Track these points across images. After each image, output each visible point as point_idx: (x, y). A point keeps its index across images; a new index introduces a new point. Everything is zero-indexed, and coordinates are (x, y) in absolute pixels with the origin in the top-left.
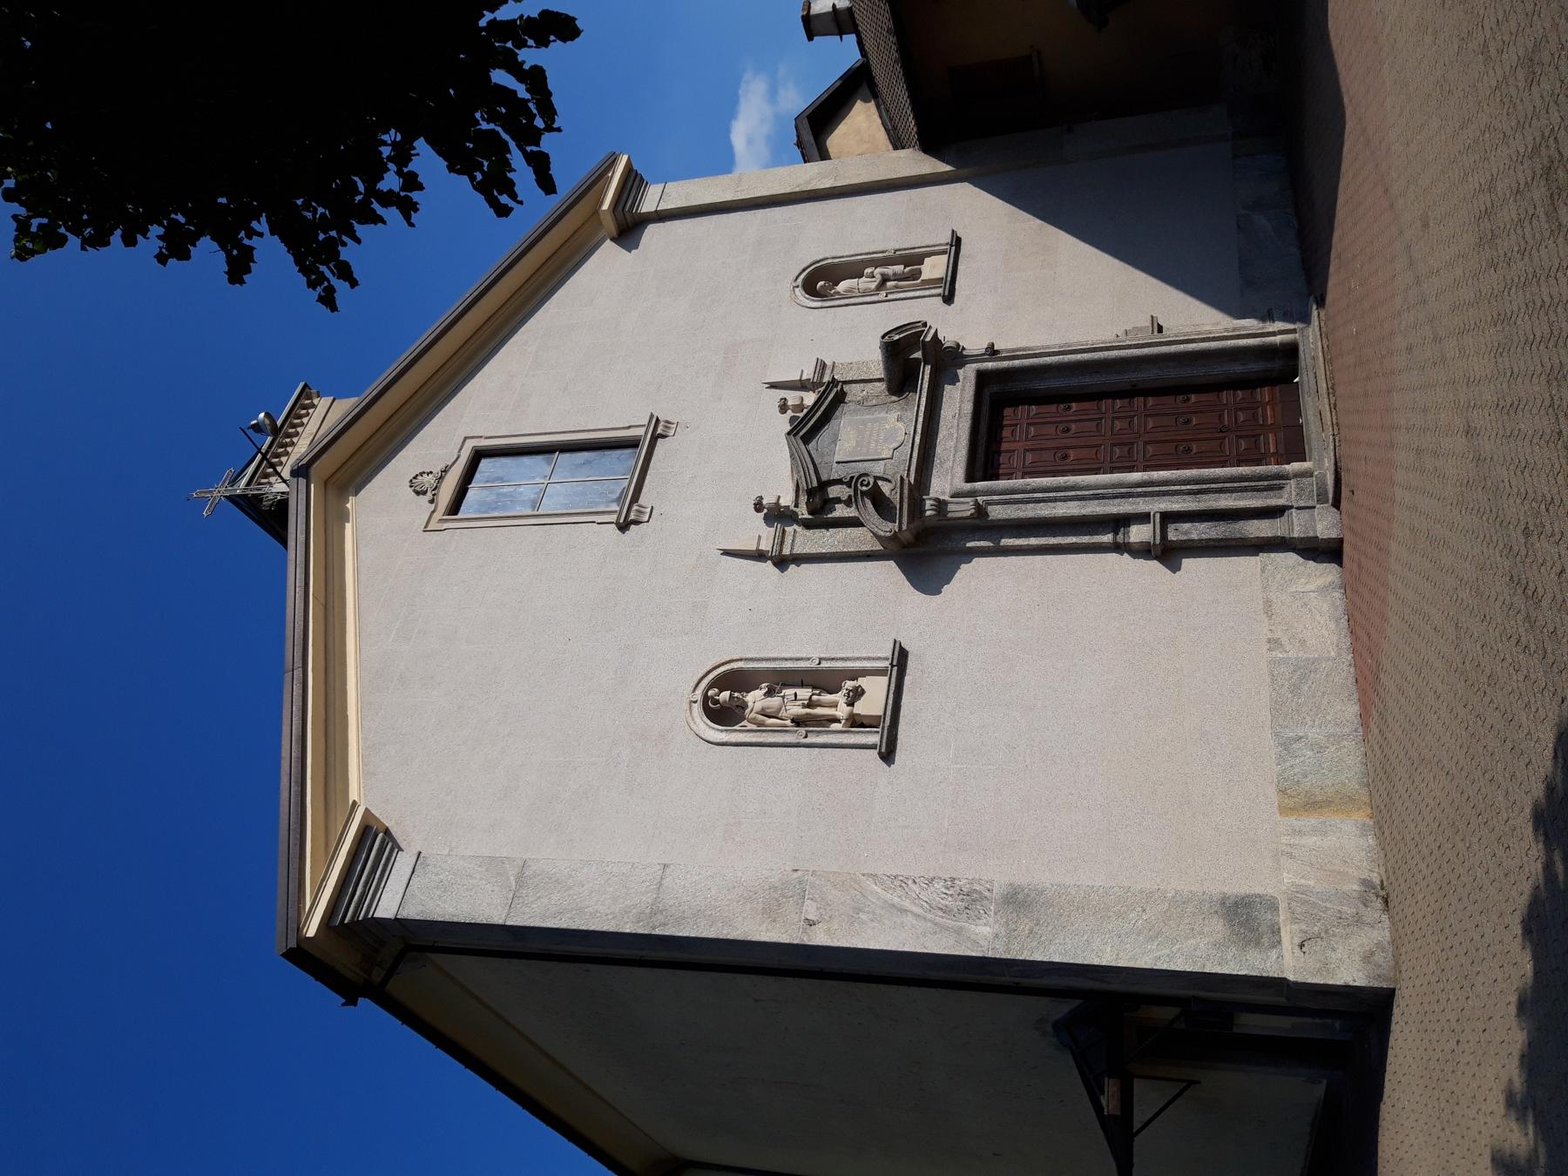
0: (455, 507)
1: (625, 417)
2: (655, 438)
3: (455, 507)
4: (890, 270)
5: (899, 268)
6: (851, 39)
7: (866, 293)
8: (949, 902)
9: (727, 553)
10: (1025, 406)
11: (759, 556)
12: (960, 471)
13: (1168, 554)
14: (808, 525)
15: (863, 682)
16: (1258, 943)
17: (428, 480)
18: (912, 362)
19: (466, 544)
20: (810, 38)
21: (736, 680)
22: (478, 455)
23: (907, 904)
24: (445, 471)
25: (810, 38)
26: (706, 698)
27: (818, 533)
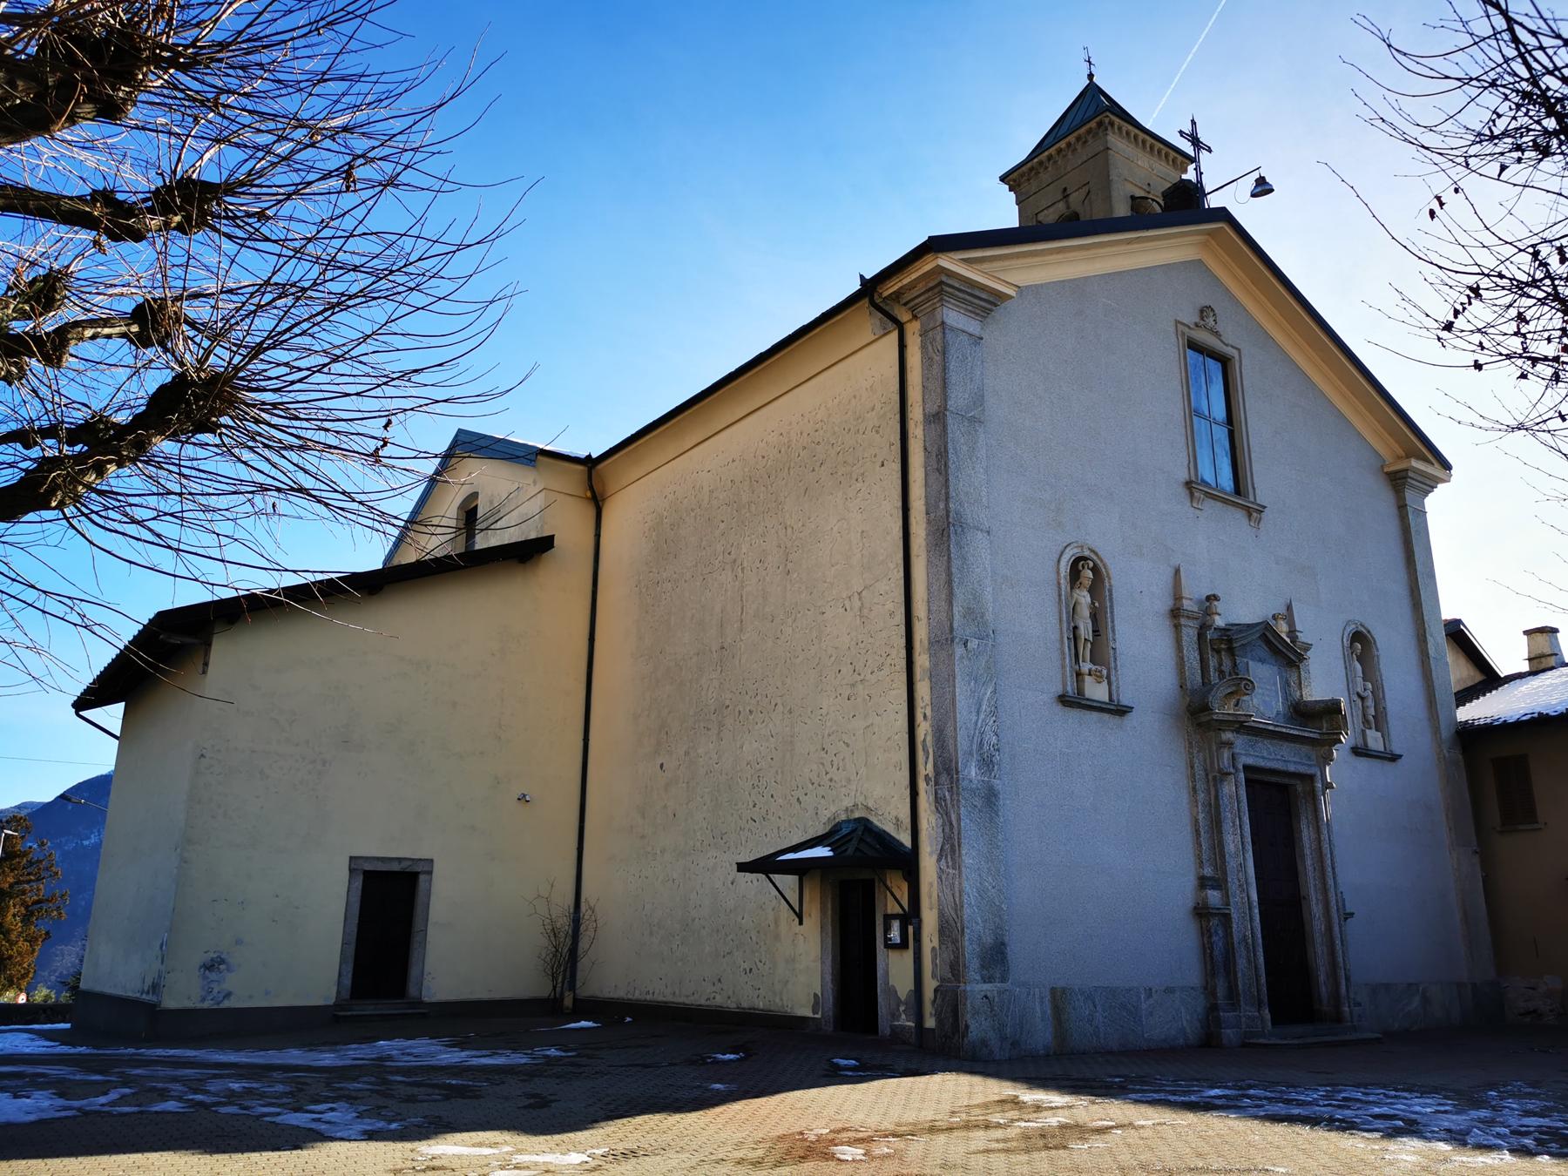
0: (1193, 345)
1: (1265, 482)
2: (1249, 512)
3: (1193, 345)
4: (1370, 703)
5: (1372, 711)
6: (1525, 667)
7: (1355, 683)
8: (986, 747)
9: (1177, 571)
10: (1279, 806)
11: (1178, 597)
12: (1250, 761)
13: (1201, 912)
14: (1201, 636)
15: (1105, 683)
16: (983, 966)
17: (1210, 321)
18: (1318, 721)
19: (1167, 358)
20: (1527, 633)
21: (1098, 586)
22: (1225, 362)
23: (982, 716)
24: (1217, 334)
25: (1527, 633)
26: (1085, 559)
27: (1542, 677)
